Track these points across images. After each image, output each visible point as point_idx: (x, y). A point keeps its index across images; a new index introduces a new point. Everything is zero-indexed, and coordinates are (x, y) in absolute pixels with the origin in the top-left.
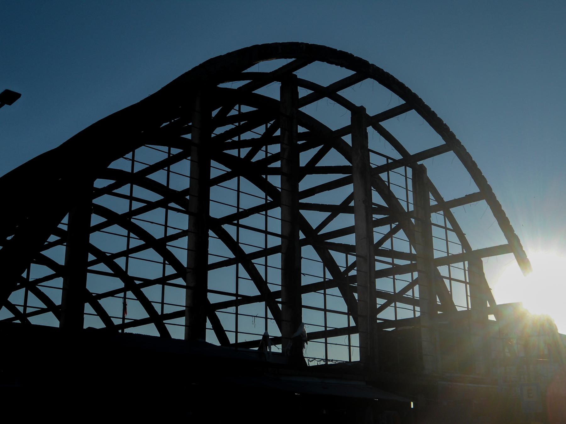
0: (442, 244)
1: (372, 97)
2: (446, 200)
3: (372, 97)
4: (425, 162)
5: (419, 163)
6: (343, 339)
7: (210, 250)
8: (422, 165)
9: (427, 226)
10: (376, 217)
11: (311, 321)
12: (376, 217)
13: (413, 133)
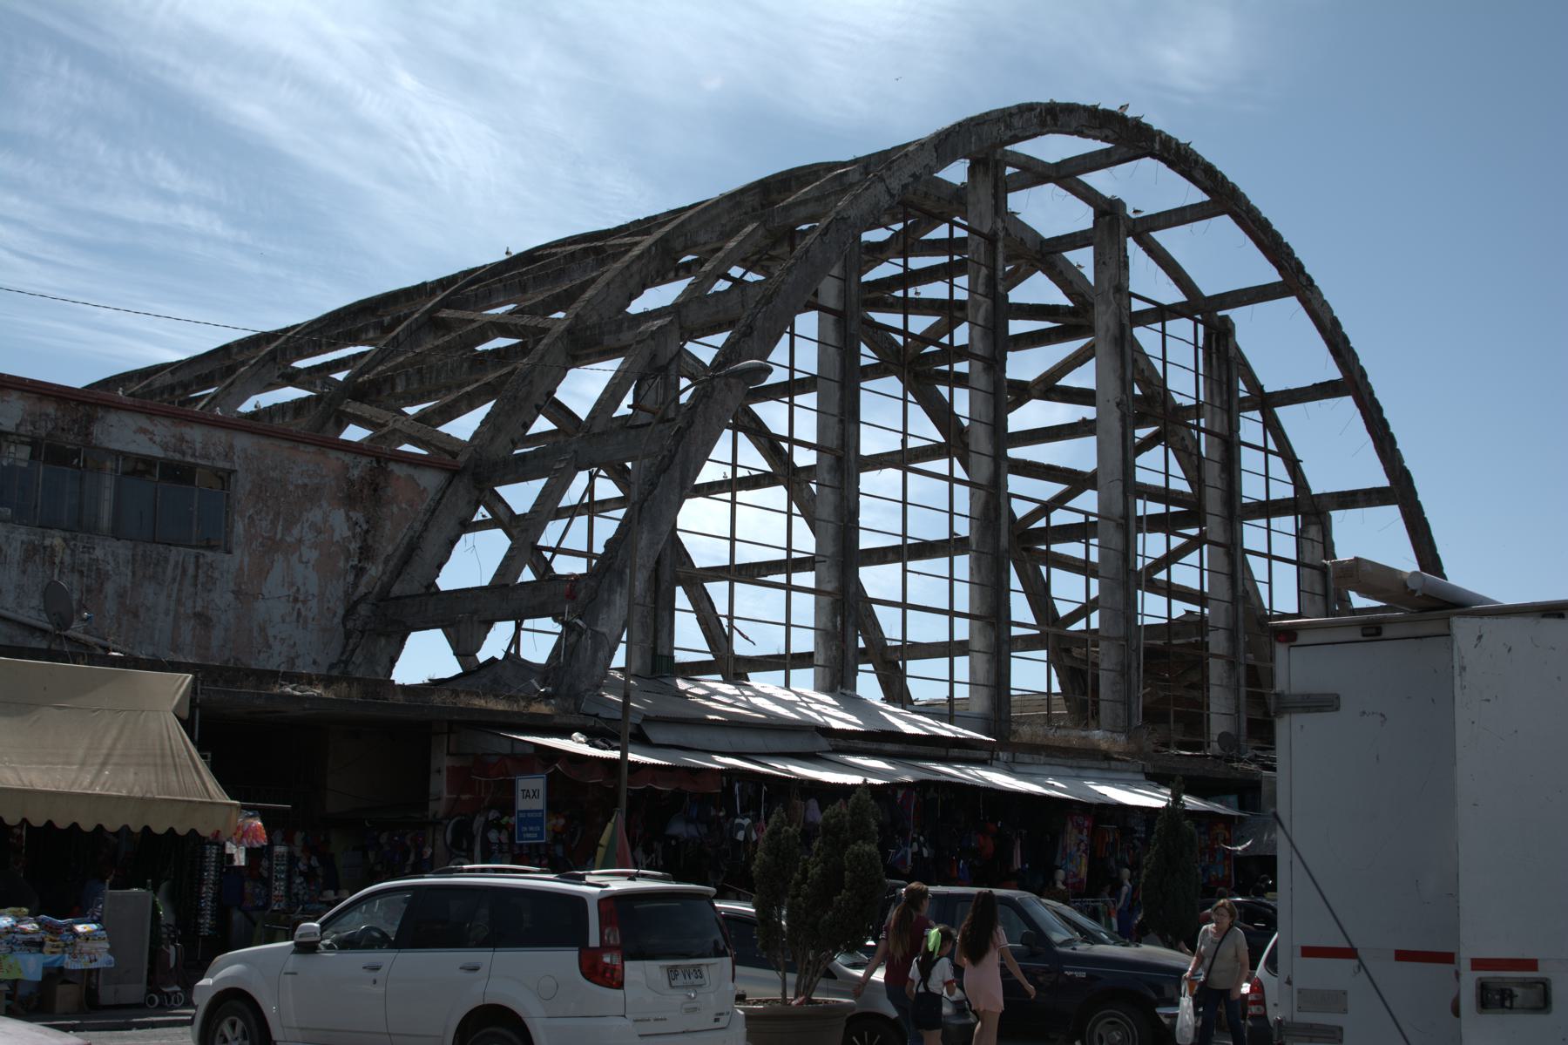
0: (1258, 478)
1: (1144, 186)
2: (1267, 389)
3: (1144, 186)
4: (1236, 315)
5: (1220, 313)
6: (939, 565)
7: (864, 520)
8: (1227, 317)
9: (1230, 446)
10: (1017, 327)
11: (877, 522)
12: (1017, 327)
13: (1218, 256)
